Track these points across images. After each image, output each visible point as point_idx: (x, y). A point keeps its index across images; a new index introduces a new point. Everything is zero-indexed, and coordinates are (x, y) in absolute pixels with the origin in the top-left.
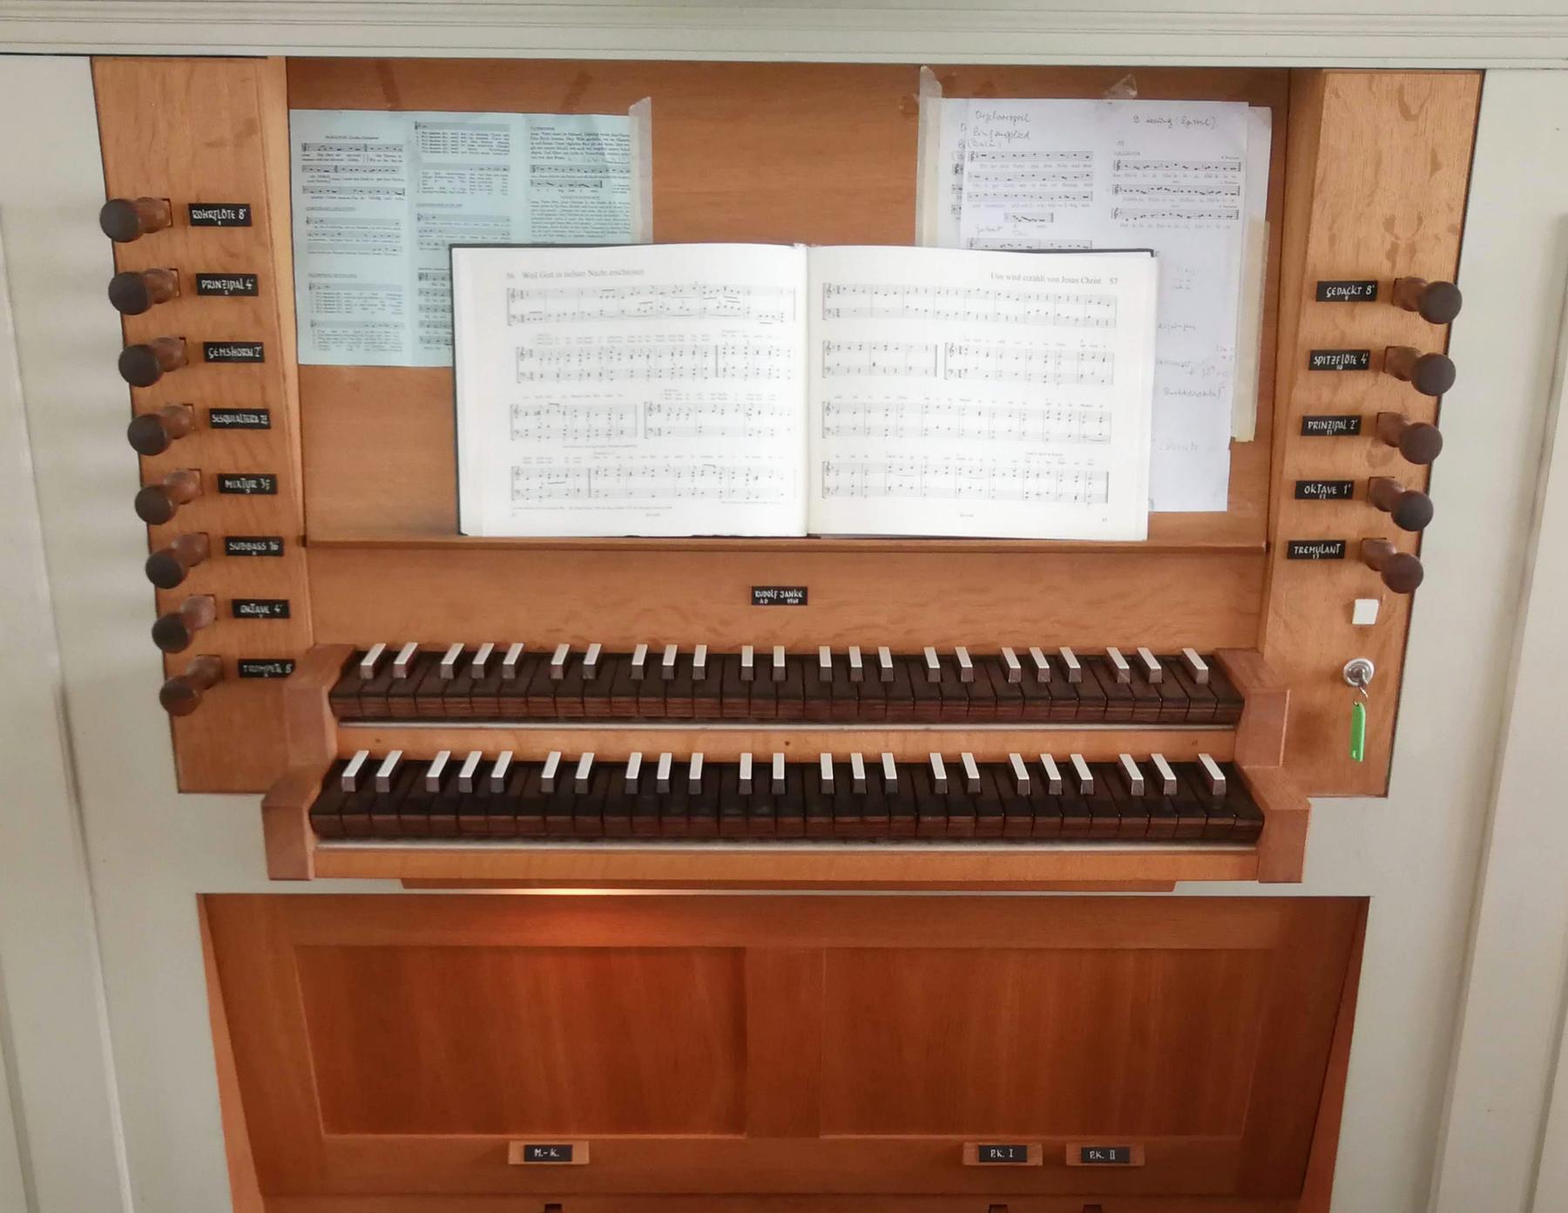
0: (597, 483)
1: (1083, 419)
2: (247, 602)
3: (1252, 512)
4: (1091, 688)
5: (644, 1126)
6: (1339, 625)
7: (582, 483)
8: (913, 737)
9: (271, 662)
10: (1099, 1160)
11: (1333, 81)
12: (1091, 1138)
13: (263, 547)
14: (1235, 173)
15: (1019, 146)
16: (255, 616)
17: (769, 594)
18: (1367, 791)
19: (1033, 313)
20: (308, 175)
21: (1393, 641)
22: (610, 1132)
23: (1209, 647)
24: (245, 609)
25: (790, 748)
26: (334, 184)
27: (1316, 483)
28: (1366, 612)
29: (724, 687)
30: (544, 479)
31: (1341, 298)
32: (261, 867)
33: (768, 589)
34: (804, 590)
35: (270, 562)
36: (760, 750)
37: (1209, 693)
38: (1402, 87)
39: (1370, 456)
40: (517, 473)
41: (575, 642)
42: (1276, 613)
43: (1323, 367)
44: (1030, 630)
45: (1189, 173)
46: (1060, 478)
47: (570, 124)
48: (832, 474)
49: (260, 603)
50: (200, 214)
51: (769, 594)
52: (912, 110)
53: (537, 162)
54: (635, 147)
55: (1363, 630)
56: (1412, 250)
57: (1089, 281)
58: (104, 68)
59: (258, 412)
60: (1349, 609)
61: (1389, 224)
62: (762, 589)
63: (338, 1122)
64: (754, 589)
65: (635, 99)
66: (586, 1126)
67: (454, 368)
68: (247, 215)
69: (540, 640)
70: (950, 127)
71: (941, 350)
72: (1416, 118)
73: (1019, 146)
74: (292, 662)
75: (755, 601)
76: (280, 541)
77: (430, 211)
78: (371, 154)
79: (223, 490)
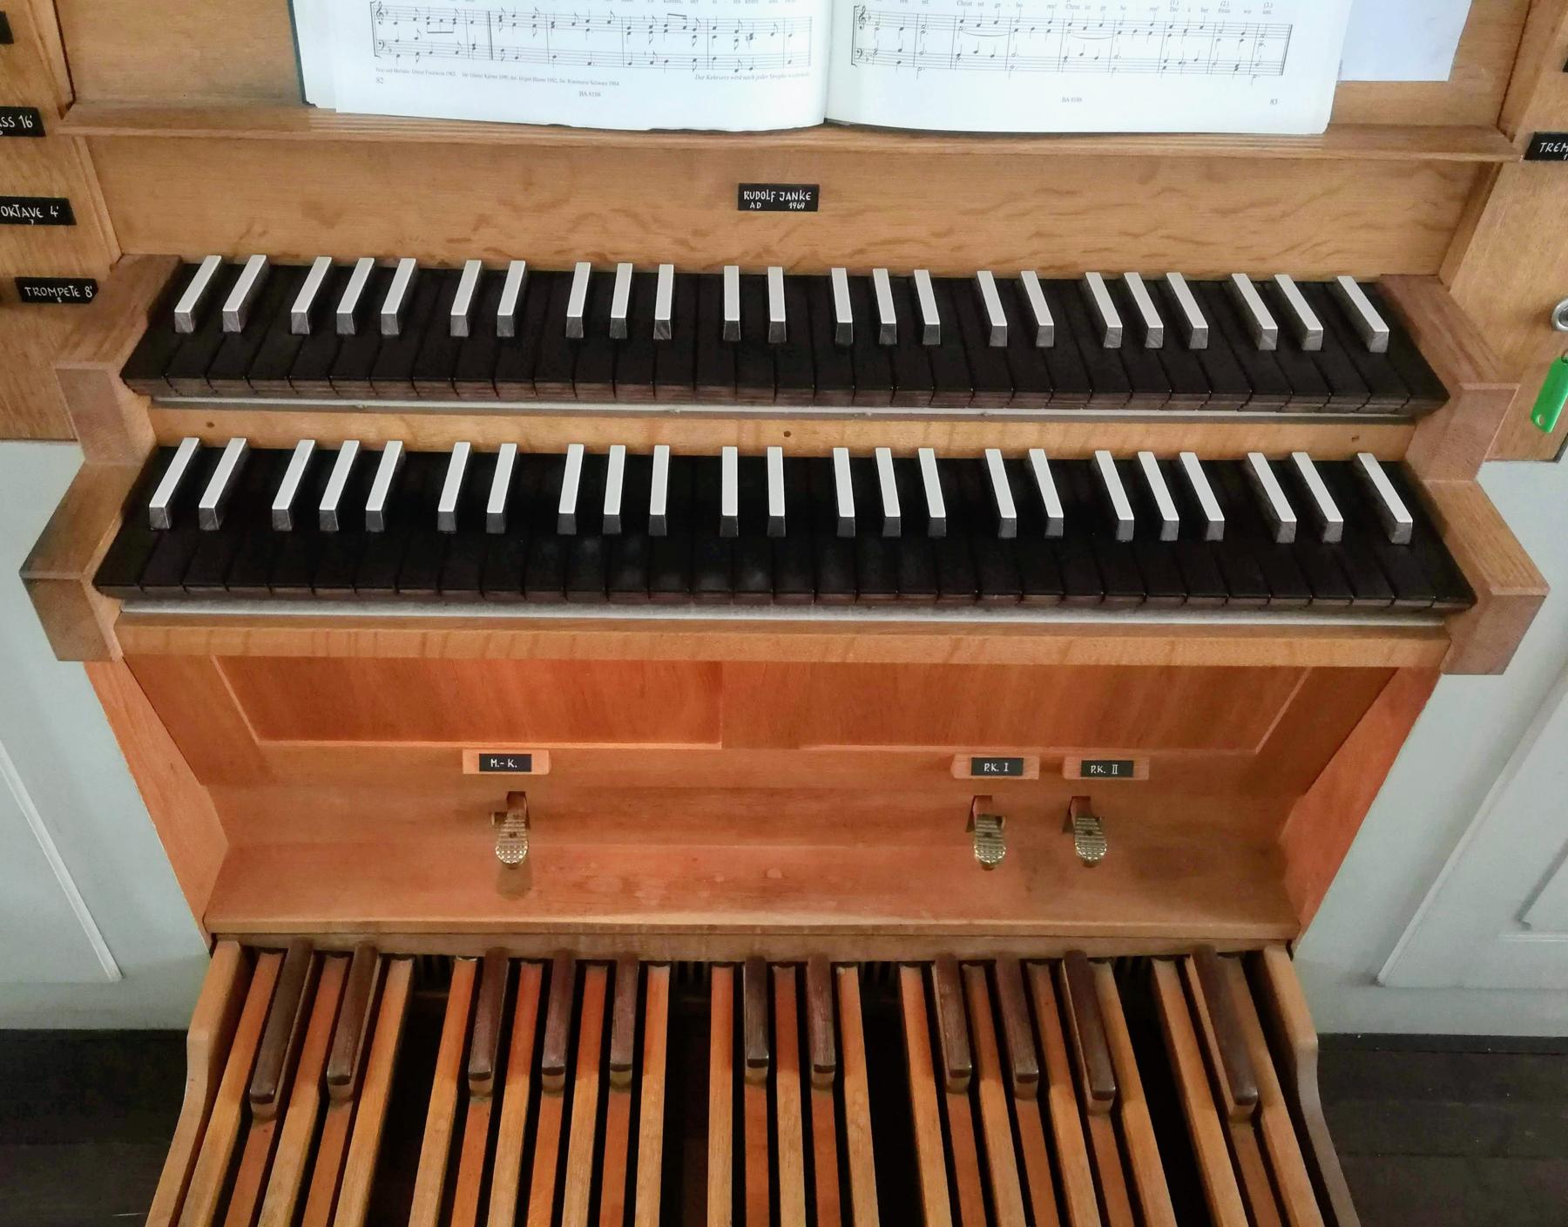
0: (503, 37)
3: (1486, 83)
4: (1218, 352)
5: (606, 732)
7: (479, 34)
8: (963, 427)
9: (64, 282)
10: (1100, 775)
16: (25, 221)
17: (764, 196)
22: (570, 740)
23: (1372, 272)
25: (792, 440)
29: (697, 345)
30: (421, 25)
34: (814, 190)
35: (26, 143)
36: (749, 442)
37: (1377, 360)
41: (491, 256)
44: (1131, 252)
48: (869, 28)
51: (764, 196)
63: (272, 732)
64: (743, 188)
66: (545, 732)
69: (440, 254)
74: (93, 283)
75: (744, 205)
76: (34, 114)
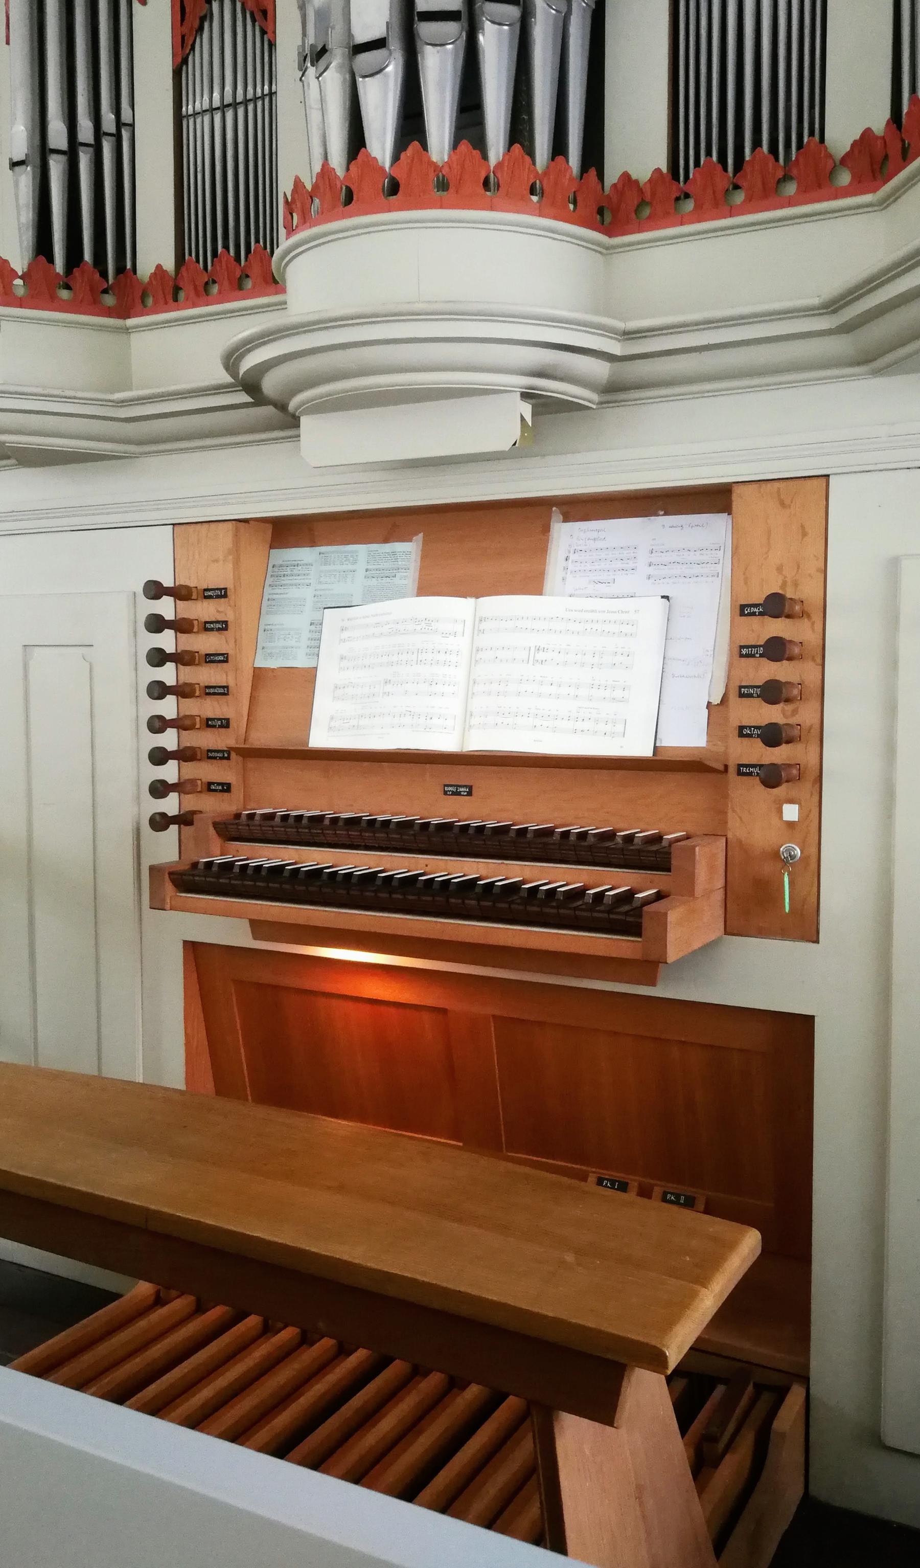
1: (614, 688)
2: (213, 783)
6: (775, 821)
11: (737, 491)
12: (670, 1185)
13: (220, 755)
14: (717, 552)
15: (600, 544)
18: (814, 942)
19: (589, 630)
20: (272, 579)
21: (810, 829)
24: (213, 787)
26: (283, 582)
27: (750, 727)
28: (791, 812)
31: (753, 614)
32: (156, 862)
33: (451, 786)
38: (779, 489)
39: (783, 712)
40: (332, 718)
42: (734, 811)
43: (748, 656)
45: (692, 553)
46: (597, 721)
47: (387, 548)
49: (219, 784)
50: (208, 594)
52: (546, 529)
53: (369, 567)
54: (413, 556)
55: (791, 825)
56: (796, 584)
57: (622, 612)
58: (177, 528)
59: (223, 687)
60: (780, 812)
61: (780, 569)
62: (448, 786)
65: (416, 534)
67: (316, 668)
68: (226, 592)
70: (566, 536)
71: (533, 650)
72: (790, 507)
73: (600, 544)
77: (321, 593)
78: (300, 568)
79: (208, 726)
